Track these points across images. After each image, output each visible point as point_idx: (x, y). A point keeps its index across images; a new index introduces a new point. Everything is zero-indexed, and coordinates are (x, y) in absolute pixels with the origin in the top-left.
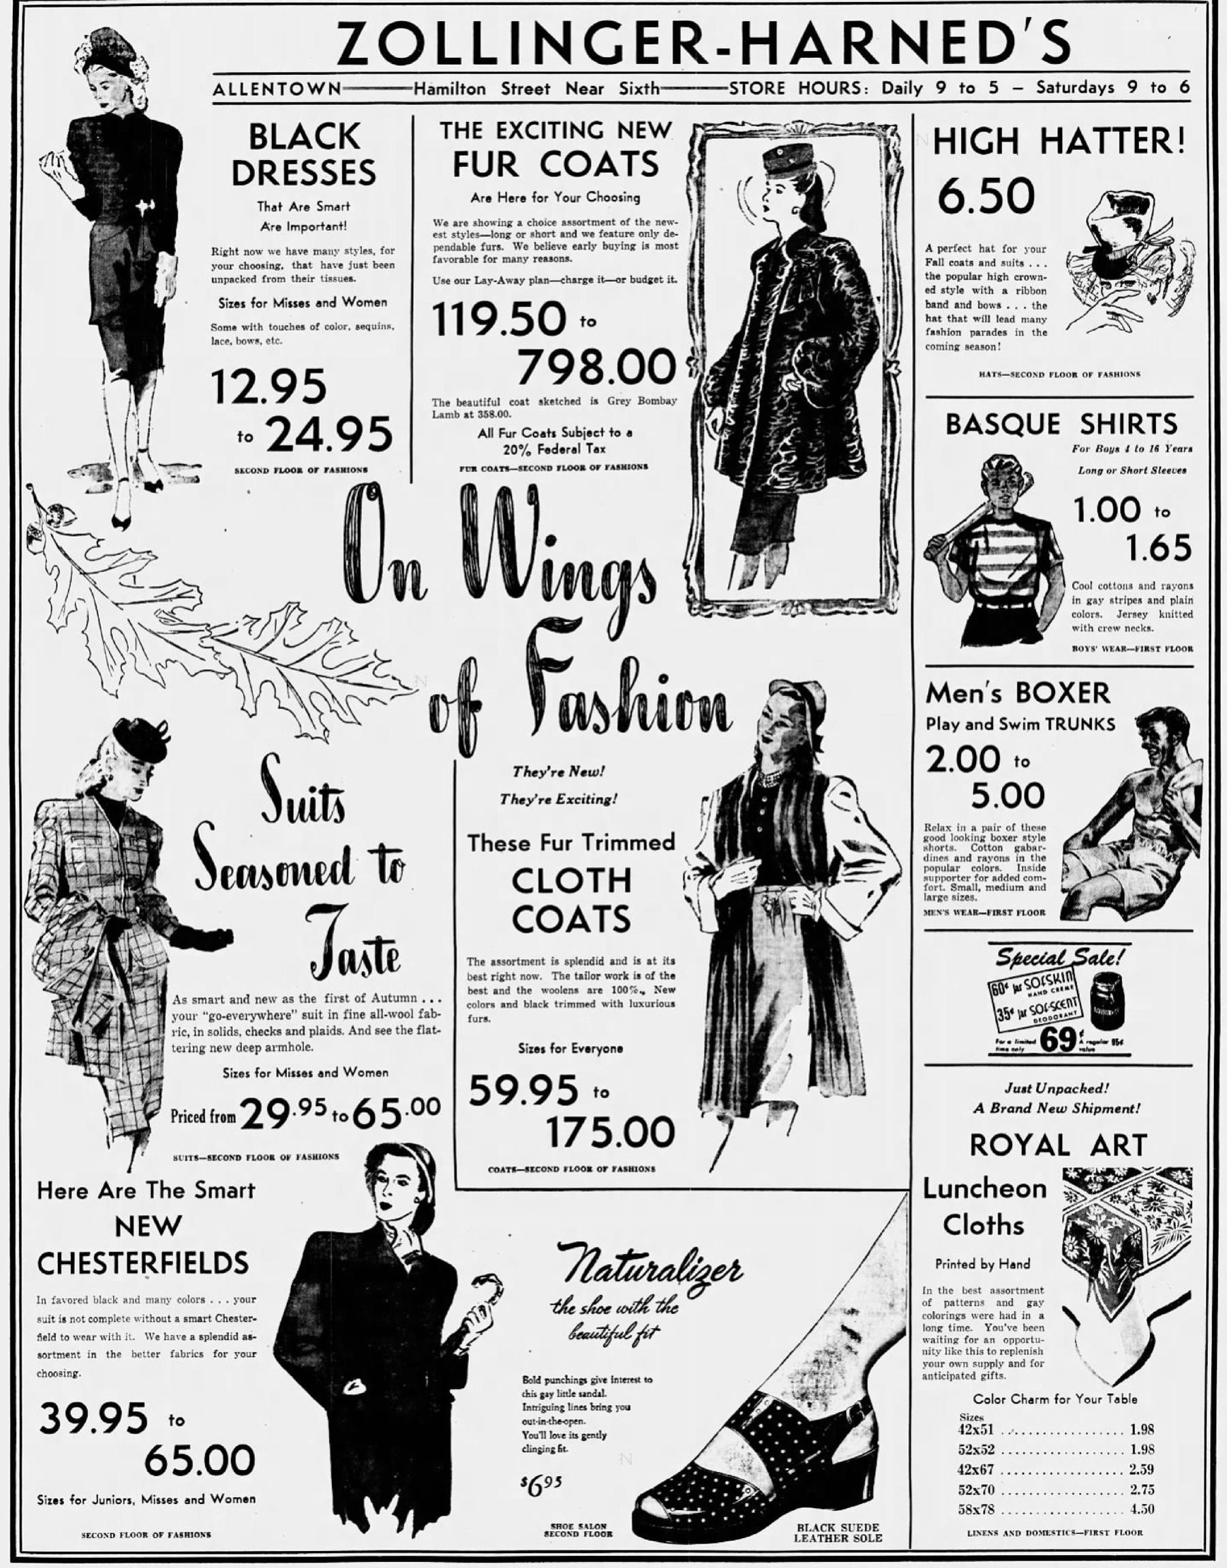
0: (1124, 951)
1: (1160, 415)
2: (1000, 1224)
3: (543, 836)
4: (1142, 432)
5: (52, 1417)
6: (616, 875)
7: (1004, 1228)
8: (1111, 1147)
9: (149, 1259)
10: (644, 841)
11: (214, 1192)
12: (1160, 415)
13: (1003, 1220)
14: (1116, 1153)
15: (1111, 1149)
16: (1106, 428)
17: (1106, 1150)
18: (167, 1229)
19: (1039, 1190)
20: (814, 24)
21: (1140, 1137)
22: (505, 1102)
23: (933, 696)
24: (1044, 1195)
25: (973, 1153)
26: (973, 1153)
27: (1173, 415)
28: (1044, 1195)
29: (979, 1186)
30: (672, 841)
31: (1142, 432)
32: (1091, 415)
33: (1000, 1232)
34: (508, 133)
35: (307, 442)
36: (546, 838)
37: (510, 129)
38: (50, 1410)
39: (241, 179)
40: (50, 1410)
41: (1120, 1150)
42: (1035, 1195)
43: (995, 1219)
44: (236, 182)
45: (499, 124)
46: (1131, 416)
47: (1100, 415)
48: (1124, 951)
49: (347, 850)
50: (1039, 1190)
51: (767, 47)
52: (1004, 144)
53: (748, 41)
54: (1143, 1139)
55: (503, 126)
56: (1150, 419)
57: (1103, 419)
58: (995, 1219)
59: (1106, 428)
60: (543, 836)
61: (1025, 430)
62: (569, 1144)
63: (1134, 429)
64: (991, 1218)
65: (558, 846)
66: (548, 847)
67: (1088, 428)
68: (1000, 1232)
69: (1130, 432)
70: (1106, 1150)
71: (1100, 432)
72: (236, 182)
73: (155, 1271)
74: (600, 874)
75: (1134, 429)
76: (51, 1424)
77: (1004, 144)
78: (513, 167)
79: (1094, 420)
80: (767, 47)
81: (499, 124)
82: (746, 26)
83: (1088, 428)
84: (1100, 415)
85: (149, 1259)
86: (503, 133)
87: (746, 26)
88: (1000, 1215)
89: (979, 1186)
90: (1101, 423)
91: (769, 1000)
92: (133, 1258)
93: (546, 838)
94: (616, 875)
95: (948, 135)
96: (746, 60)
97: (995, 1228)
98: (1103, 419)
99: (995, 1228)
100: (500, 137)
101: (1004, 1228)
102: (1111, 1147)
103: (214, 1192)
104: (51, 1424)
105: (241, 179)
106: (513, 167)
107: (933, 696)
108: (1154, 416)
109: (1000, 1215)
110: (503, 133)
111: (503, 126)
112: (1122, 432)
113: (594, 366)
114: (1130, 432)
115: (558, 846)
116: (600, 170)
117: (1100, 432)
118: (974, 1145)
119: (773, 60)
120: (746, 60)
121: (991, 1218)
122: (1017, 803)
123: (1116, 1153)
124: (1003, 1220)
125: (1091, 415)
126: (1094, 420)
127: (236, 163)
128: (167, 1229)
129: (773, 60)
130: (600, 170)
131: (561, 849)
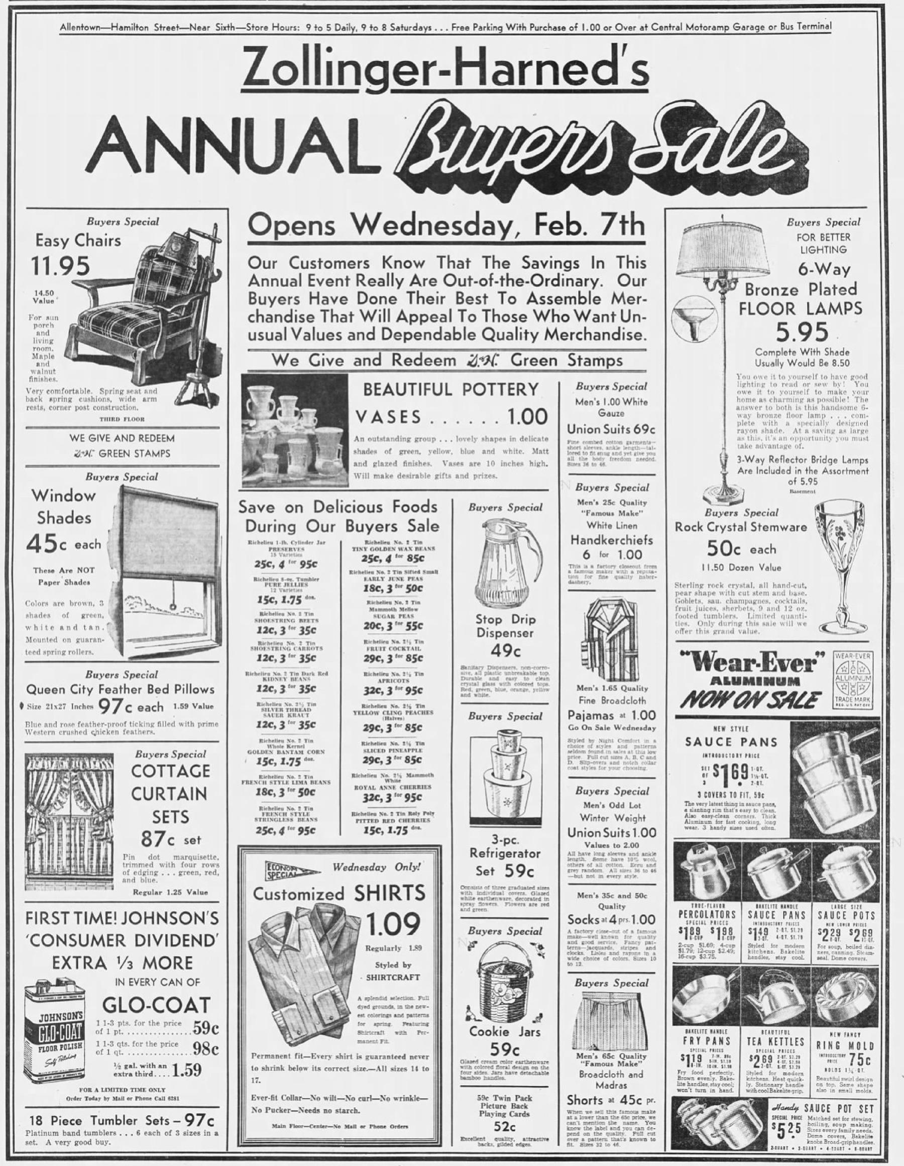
0: (605, 233)
1: (412, 886)
4: (399, 899)
12: (412, 886)
16: (373, 896)
19: (299, 508)
20: (185, 173)
21: (205, 999)
22: (411, 933)
27: (422, 886)
29: (252, 315)
30: (342, 893)
31: (399, 899)
32: (362, 886)
34: (60, 965)
35: (32, 548)
37: (62, 962)
43: (628, 218)
45: (54, 957)
46: (391, 886)
47: (369, 886)
48: (605, 233)
50: (299, 508)
51: (477, 70)
52: (465, 70)
53: (461, 64)
54: (208, 1001)
55: (57, 960)
56: (406, 888)
57: (371, 889)
59: (373, 896)
61: (495, 338)
62: (157, 845)
63: (394, 897)
66: (398, 509)
67: (360, 896)
69: (391, 899)
71: (369, 899)
75: (394, 897)
77: (465, 70)
79: (364, 890)
81: (54, 957)
82: (459, 50)
83: (360, 896)
84: (369, 886)
86: (57, 965)
87: (459, 50)
89: (252, 315)
90: (369, 892)
96: (459, 81)
98: (371, 889)
100: (55, 968)
105: (208, 943)
108: (408, 887)
110: (57, 965)
111: (57, 960)
112: (385, 899)
114: (391, 899)
117: (369, 899)
118: (394, 360)
119: (483, 81)
120: (459, 81)
125: (362, 886)
126: (364, 890)
129: (483, 81)
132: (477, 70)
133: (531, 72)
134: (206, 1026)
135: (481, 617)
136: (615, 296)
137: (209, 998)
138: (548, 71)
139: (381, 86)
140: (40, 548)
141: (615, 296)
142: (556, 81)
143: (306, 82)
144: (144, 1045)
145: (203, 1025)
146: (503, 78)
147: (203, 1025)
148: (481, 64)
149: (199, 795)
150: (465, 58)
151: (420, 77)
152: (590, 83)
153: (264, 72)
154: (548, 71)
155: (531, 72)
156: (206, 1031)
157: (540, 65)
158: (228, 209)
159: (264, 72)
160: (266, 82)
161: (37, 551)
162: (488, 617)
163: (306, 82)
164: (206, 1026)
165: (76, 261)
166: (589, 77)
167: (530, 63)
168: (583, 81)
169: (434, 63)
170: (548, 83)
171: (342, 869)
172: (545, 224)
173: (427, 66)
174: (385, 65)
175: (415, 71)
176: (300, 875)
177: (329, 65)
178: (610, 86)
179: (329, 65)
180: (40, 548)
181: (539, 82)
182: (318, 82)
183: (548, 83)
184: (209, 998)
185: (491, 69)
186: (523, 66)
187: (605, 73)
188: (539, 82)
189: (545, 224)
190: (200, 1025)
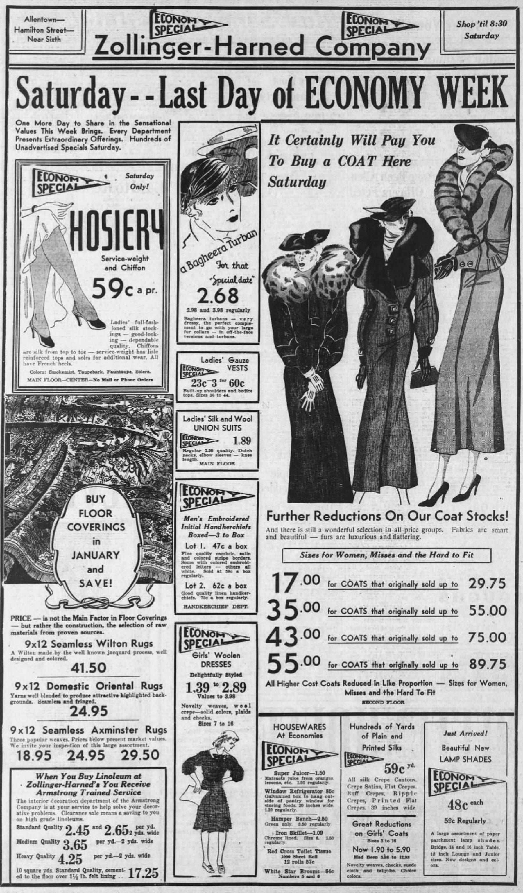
2: (292, 515)
3: (268, 512)
5: (275, 609)
7: (294, 517)
13: (294, 513)
25: (315, 519)
26: (315, 519)
29: (491, 515)
33: (292, 519)
35: (273, 641)
36: (270, 514)
38: (274, 605)
40: (274, 605)
43: (290, 513)
49: (302, 36)
51: (227, 47)
53: (218, 44)
58: (290, 513)
60: (268, 512)
65: (277, 518)
66: (271, 519)
67: (470, 518)
82: (217, 38)
87: (217, 38)
89: (491, 515)
91: (25, 239)
93: (270, 514)
96: (217, 52)
97: (290, 517)
99: (290, 517)
101: (294, 517)
104: (274, 614)
109: (292, 511)
113: (235, 295)
115: (277, 518)
118: (315, 516)
119: (229, 53)
120: (217, 52)
122: (495, 640)
124: (294, 513)
129: (229, 53)
131: (278, 519)
132: (227, 47)
133: (257, 49)
134: (395, 767)
135: (473, 514)
138: (266, 48)
139: (171, 55)
140: (280, 641)
142: (270, 53)
143: (129, 52)
144: (136, 380)
145: (393, 766)
146: (241, 51)
147: (393, 766)
148: (229, 45)
150: (220, 42)
151: (192, 51)
152: (289, 54)
153: (106, 47)
154: (266, 48)
155: (257, 49)
156: (395, 771)
157: (262, 45)
158: (8, 8)
159: (106, 47)
160: (106, 53)
161: (278, 645)
162: (479, 514)
163: (129, 52)
164: (395, 767)
165: (97, 753)
166: (288, 51)
167: (256, 44)
168: (285, 53)
169: (200, 44)
170: (265, 54)
171: (343, 556)
173: (196, 45)
175: (189, 48)
176: (479, 785)
177: (143, 44)
178: (299, 56)
179: (143, 44)
180: (280, 641)
181: (261, 53)
182: (136, 52)
183: (265, 54)
185: (234, 47)
186: (252, 45)
187: (297, 49)
188: (261, 53)
190: (390, 766)
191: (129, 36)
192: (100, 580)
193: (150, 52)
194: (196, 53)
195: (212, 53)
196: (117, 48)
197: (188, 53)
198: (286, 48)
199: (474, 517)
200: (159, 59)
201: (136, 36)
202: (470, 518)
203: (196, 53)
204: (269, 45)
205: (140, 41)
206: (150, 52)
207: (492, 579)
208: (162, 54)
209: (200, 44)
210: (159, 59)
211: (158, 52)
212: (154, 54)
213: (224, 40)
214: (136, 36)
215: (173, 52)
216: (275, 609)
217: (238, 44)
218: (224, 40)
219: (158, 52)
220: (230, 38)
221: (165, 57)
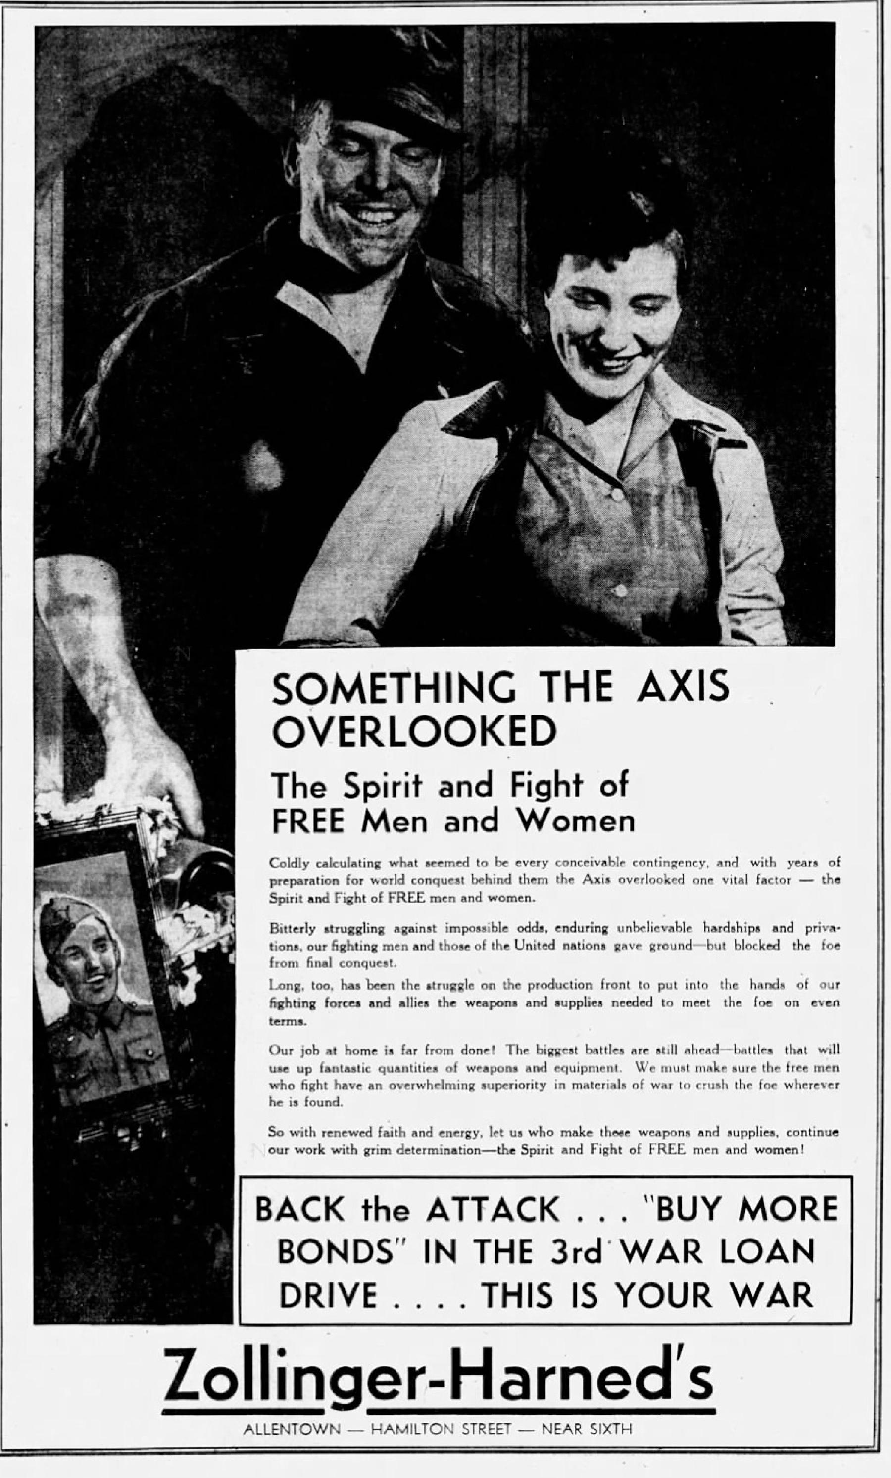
2: (377, 1208)
3: (514, 774)
5: (561, 1251)
6: (501, 1246)
7: (382, 1213)
8: (790, 1298)
9: (298, 816)
10: (317, 1372)
11: (580, 823)
13: (381, 1204)
14: (796, 1304)
15: (790, 1299)
17: (784, 1301)
18: (533, 824)
23: (369, 824)
24: (632, 829)
28: (632, 829)
33: (377, 1218)
38: (560, 1245)
39: (360, 1257)
40: (560, 1245)
41: (800, 1301)
42: (575, 829)
43: (372, 1203)
44: (284, 1305)
48: (742, 445)
49: (490, 772)
51: (480, 1378)
54: (484, 1203)
58: (372, 1203)
60: (514, 774)
64: (366, 1201)
68: (377, 1218)
70: (784, 1301)
72: (284, 1305)
73: (321, 1305)
74: (486, 1245)
76: (560, 1257)
78: (697, 1254)
80: (480, 1378)
82: (456, 1352)
85: (298, 816)
87: (456, 1352)
88: (377, 1198)
92: (518, 724)
94: (501, 1246)
95: (507, 1246)
97: (372, 1212)
99: (372, 1212)
101: (382, 1213)
102: (790, 1298)
103: (580, 823)
104: (560, 1257)
105: (360, 1257)
106: (697, 1254)
107: (369, 824)
109: (377, 1198)
116: (771, 1257)
119: (487, 1394)
121: (366, 1201)
123: (796, 1304)
124: (381, 1204)
127: (284, 1285)
128: (533, 824)
129: (487, 1394)
130: (771, 1257)
133: (553, 1383)
136: (745, 1205)
137: (486, 1198)
138: (576, 1381)
141: (745, 1205)
143: (248, 1395)
148: (485, 1371)
149: (341, 1248)
151: (403, 1389)
152: (634, 1399)
153: (193, 1382)
155: (553, 1383)
157: (566, 1373)
159: (193, 1382)
160: (194, 1396)
166: (632, 1388)
167: (553, 1371)
168: (624, 1394)
169: (423, 1371)
172: (522, 784)
173: (413, 1374)
174: (356, 1372)
177: (282, 1372)
179: (282, 1372)
184: (486, 1198)
185: (499, 1378)
187: (654, 1383)
189: (522, 784)
191: (248, 1349)
192: (688, 673)
193: (298, 1395)
194: (412, 1395)
195: (442, 1398)
196: (221, 1384)
197: (394, 1394)
198: (627, 1381)
199: (619, 787)
200: (321, 1412)
201: (265, 1349)
202: (283, 696)
203: (412, 1395)
204: (584, 1372)
205: (275, 1362)
206: (298, 1395)
207: (169, 1352)
208: (330, 1397)
209: (423, 1371)
210: (321, 1412)
211: (320, 1395)
212: (309, 1400)
213: (472, 1358)
214: (265, 1349)
215: (356, 1394)
216: (561, 1251)
217: (509, 1370)
218: (472, 1358)
219: (320, 1395)
220: (488, 1352)
221: (336, 1406)
